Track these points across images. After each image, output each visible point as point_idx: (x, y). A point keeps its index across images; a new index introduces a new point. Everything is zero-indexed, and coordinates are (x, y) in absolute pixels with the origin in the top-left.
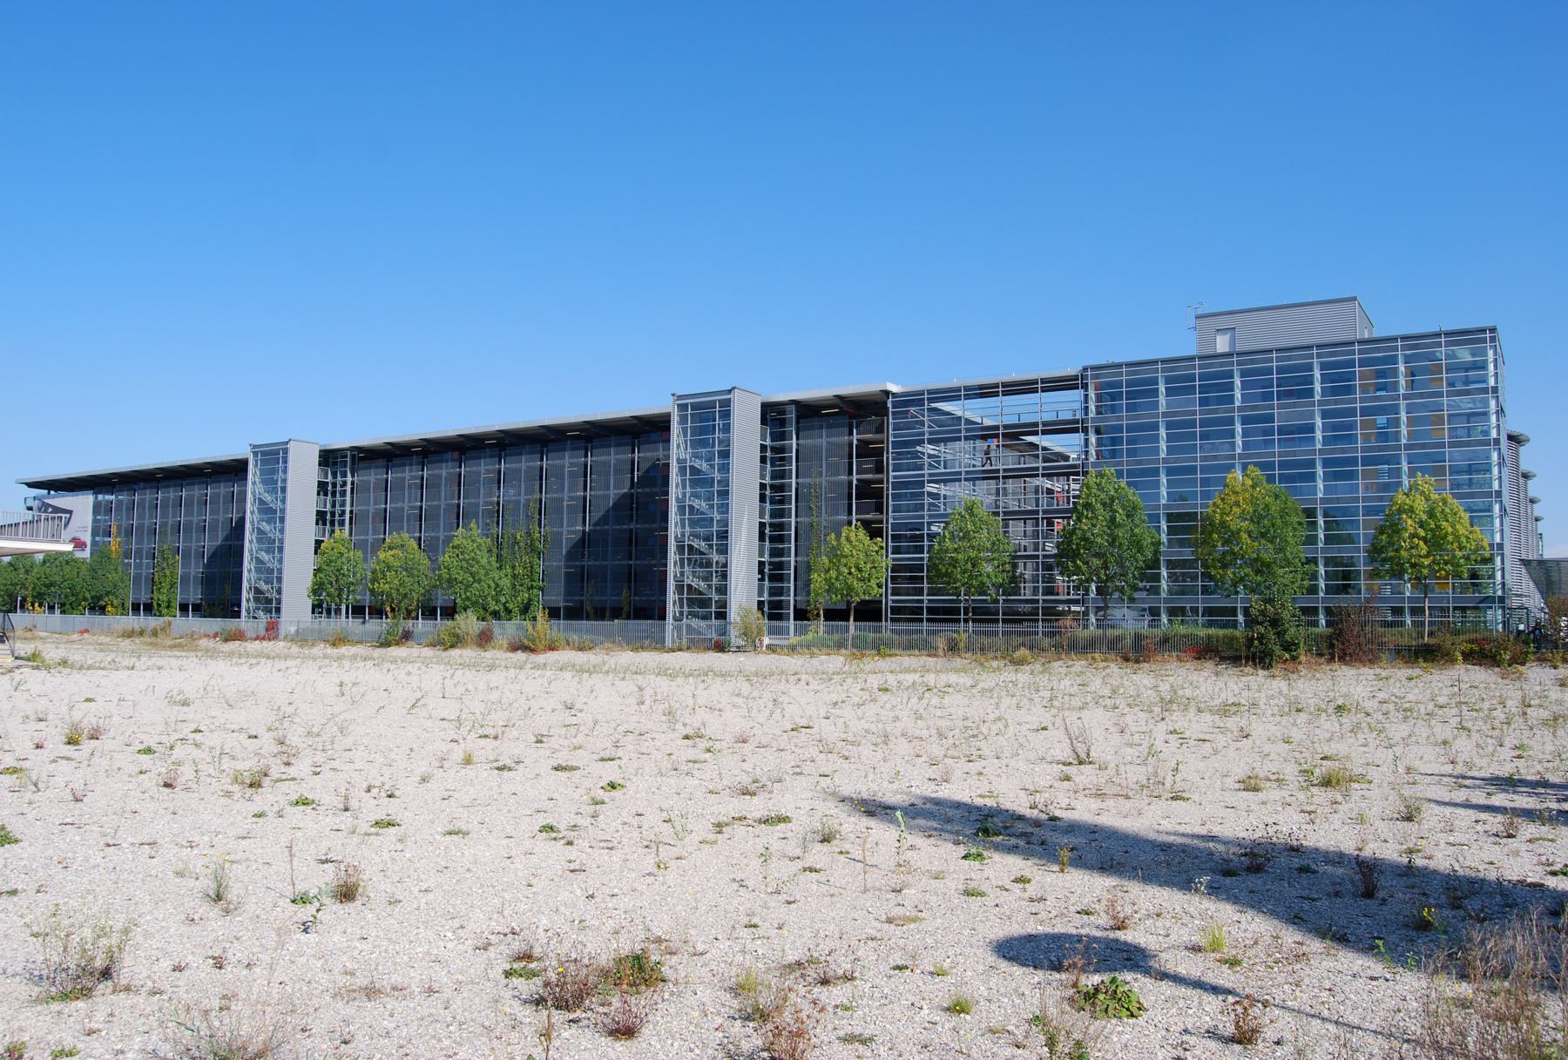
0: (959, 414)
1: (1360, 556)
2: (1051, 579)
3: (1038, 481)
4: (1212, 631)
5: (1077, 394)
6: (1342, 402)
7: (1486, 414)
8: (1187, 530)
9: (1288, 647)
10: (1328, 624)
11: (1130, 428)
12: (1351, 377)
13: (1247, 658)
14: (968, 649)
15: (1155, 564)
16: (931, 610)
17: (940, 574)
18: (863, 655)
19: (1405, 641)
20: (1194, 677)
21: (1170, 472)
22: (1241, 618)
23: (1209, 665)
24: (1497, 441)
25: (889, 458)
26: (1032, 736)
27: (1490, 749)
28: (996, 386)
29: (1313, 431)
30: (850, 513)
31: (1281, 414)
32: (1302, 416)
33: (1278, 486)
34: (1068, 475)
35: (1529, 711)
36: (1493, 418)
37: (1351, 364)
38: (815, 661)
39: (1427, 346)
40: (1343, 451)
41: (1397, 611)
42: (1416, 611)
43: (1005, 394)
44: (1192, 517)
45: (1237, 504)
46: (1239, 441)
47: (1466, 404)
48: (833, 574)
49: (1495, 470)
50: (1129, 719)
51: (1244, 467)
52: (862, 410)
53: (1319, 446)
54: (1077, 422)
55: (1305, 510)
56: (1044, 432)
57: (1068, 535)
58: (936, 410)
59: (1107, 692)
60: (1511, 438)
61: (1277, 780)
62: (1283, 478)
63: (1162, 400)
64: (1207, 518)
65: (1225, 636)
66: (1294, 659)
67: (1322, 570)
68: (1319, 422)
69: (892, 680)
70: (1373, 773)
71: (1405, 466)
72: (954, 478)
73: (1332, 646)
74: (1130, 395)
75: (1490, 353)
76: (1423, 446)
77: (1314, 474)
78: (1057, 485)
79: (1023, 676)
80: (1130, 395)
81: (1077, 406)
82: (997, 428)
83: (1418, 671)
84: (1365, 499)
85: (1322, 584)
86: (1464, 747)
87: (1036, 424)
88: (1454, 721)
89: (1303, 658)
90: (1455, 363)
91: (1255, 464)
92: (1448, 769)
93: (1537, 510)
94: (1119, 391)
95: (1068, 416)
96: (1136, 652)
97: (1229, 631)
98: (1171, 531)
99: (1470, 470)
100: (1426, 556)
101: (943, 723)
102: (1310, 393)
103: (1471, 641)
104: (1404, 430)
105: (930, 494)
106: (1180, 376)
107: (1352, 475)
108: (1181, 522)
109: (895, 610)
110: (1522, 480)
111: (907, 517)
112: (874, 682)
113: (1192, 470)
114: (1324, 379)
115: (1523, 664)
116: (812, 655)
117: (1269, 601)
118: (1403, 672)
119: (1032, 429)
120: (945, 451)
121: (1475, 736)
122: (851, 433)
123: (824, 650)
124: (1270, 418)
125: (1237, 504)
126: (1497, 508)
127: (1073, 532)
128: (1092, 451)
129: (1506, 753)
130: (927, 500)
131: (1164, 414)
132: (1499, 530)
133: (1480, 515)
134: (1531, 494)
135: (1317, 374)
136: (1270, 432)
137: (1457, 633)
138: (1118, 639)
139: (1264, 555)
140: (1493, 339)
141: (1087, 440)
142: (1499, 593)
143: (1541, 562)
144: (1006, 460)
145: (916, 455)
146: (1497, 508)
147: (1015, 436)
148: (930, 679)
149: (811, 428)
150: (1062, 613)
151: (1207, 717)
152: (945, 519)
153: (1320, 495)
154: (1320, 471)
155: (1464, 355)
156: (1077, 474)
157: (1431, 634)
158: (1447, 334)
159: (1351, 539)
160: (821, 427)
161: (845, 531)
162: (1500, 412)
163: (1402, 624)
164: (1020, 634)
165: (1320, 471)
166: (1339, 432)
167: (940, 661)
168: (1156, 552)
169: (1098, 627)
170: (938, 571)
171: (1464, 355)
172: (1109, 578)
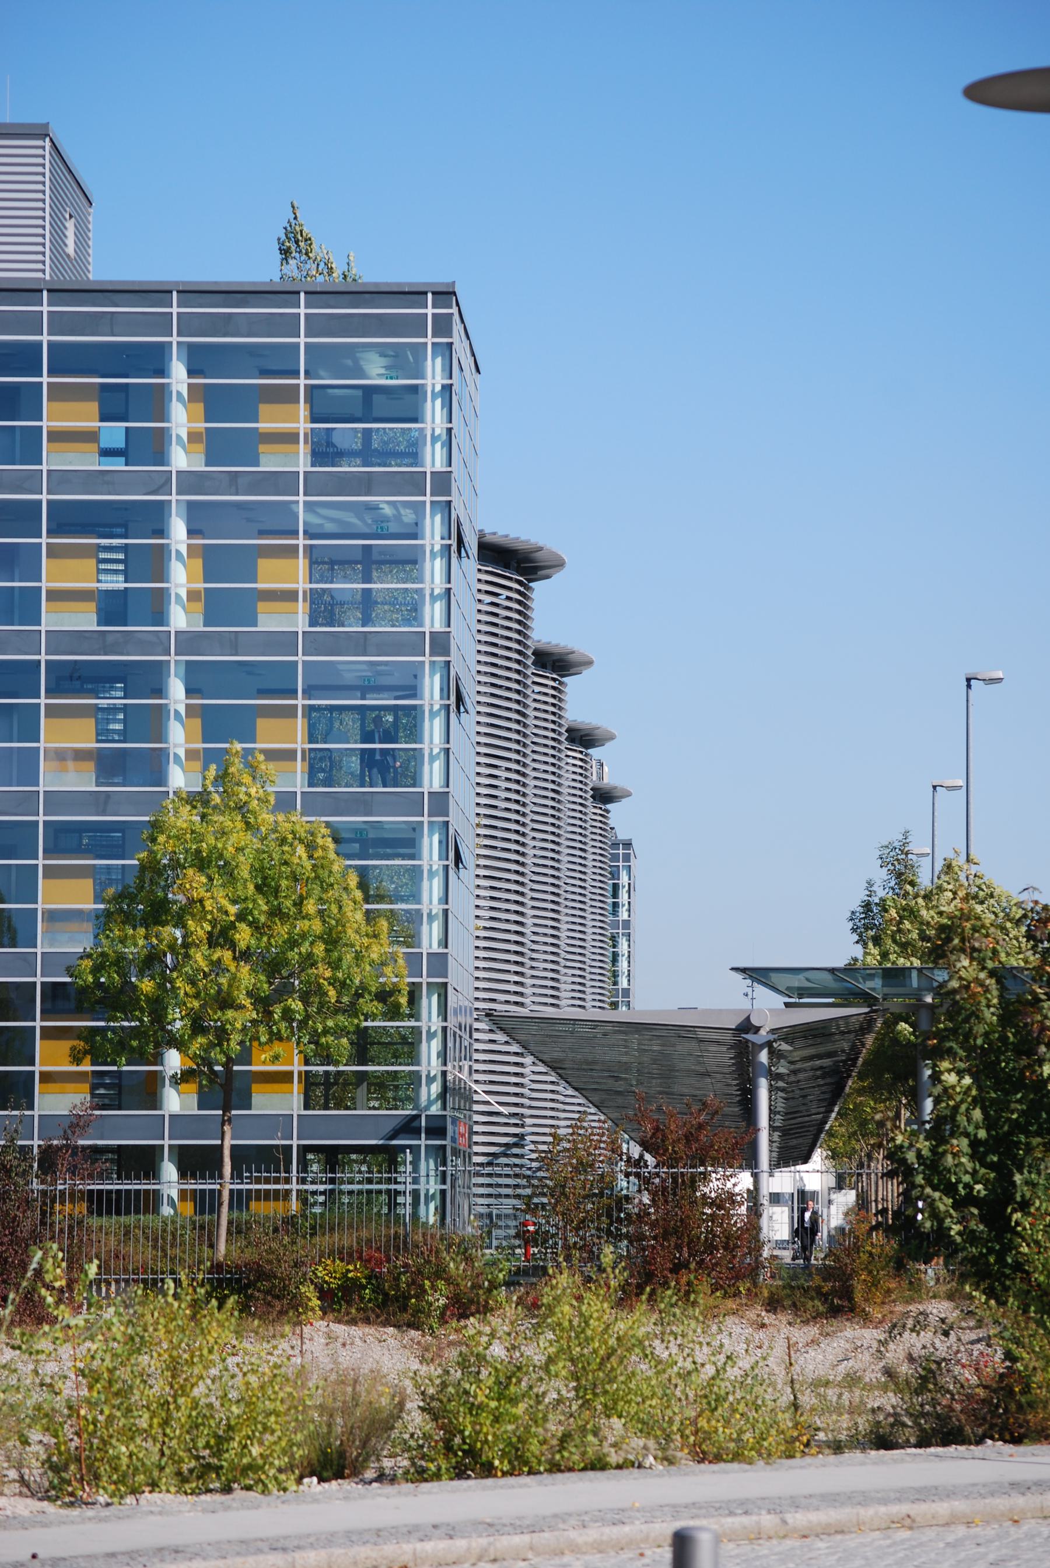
49: (433, 731)
163: (151, 1202)
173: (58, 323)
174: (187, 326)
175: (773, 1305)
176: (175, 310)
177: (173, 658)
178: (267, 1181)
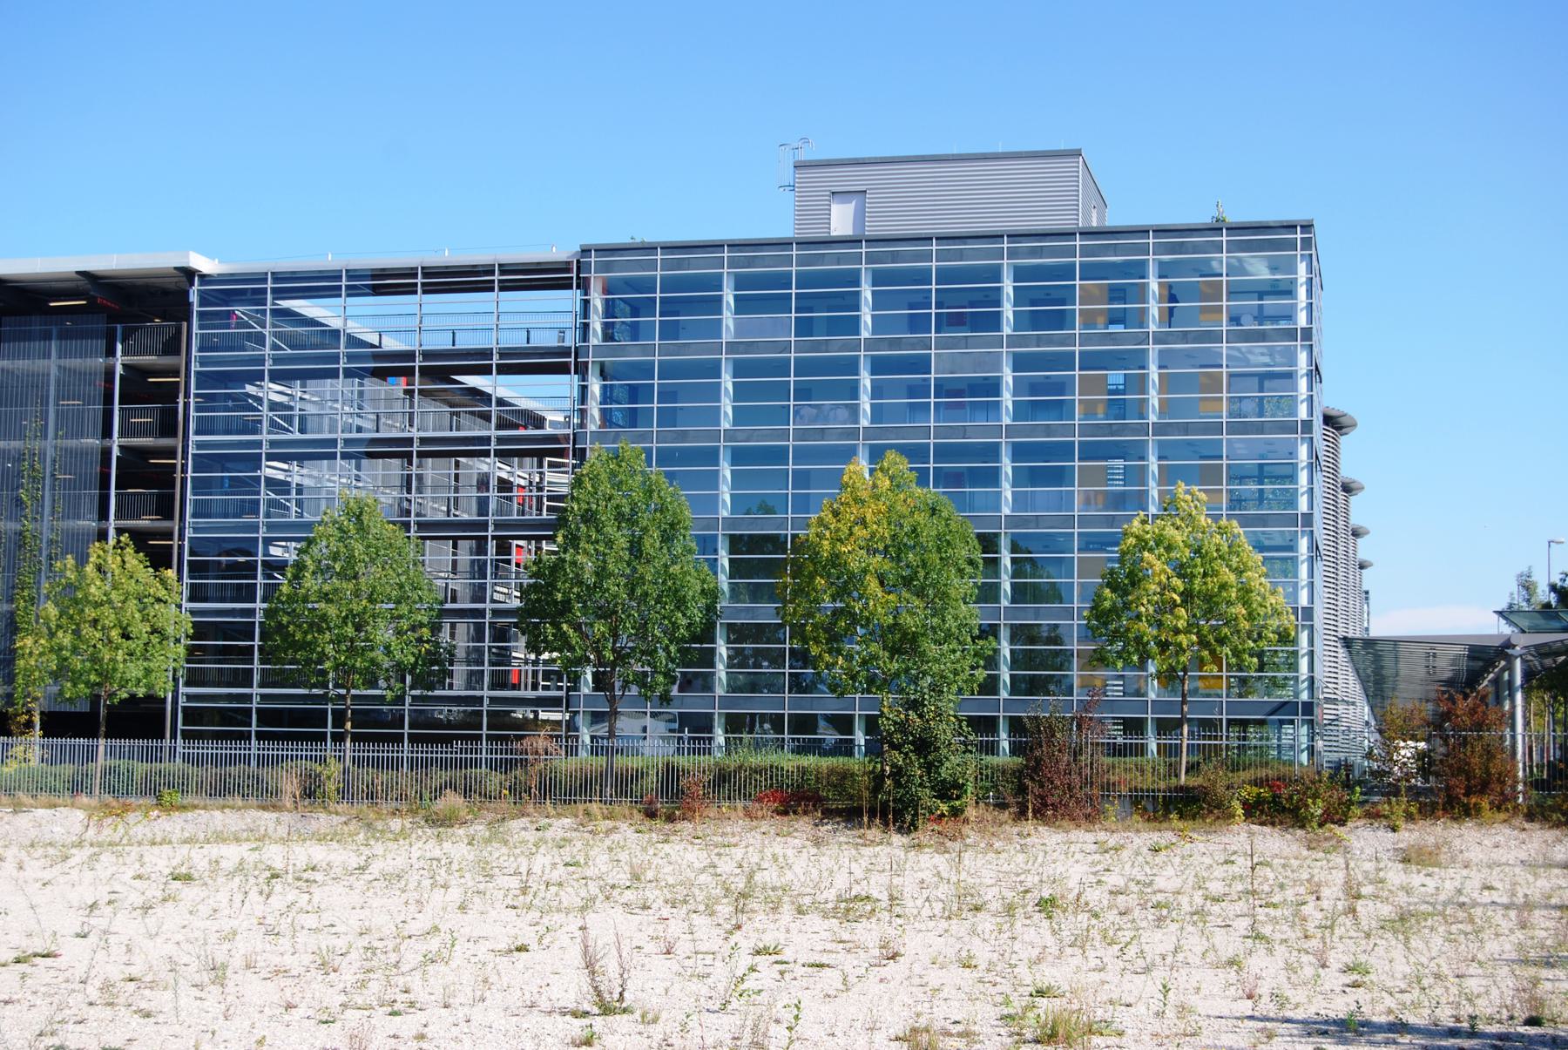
0: (335, 324)
1: (1072, 618)
2: (503, 657)
3: (483, 466)
4: (810, 761)
5: (567, 300)
6: (1050, 341)
7: (1290, 376)
8: (772, 568)
9: (948, 790)
10: (1016, 750)
11: (668, 370)
12: (1066, 296)
13: (872, 815)
14: (345, 793)
15: (707, 634)
16: (265, 717)
17: (286, 643)
18: (126, 808)
19: (1147, 782)
20: (777, 846)
21: (738, 456)
22: (860, 738)
23: (803, 825)
24: (1307, 426)
25: (189, 405)
26: (504, 961)
27: (1308, 972)
28: (411, 273)
29: (997, 393)
30: (103, 515)
31: (944, 356)
32: (979, 363)
33: (932, 492)
34: (540, 455)
35: (1359, 905)
36: (1303, 384)
37: (1067, 272)
38: (23, 820)
39: (1196, 248)
40: (1048, 431)
41: (1134, 726)
42: (1164, 727)
43: (429, 289)
44: (776, 543)
45: (863, 522)
46: (865, 403)
47: (1259, 356)
48: (66, 639)
49: (1303, 477)
50: (676, 928)
51: (876, 454)
52: (135, 306)
53: (1006, 420)
54: (565, 352)
55: (981, 538)
56: (504, 370)
57: (547, 577)
58: (287, 313)
59: (623, 878)
60: (1329, 420)
61: (965, 1034)
62: (944, 478)
63: (728, 318)
64: (799, 545)
65: (832, 771)
66: (956, 813)
67: (1006, 649)
68: (1008, 376)
69: (199, 859)
70: (1124, 1018)
71: (1153, 464)
72: (320, 452)
73: (1022, 790)
74: (669, 307)
75: (1302, 268)
76: (1186, 429)
77: (997, 471)
78: (520, 474)
79: (456, 847)
80: (669, 307)
81: (568, 321)
82: (410, 356)
83: (1169, 836)
84: (1083, 521)
85: (1005, 675)
86: (1266, 968)
87: (487, 353)
88: (1243, 924)
89: (971, 812)
90: (1245, 275)
91: (903, 450)
92: (1246, 1007)
93: (1364, 549)
94: (648, 294)
95: (548, 340)
96: (668, 800)
97: (838, 762)
98: (737, 569)
99: (1261, 474)
100: (1187, 631)
101: (325, 940)
102: (994, 321)
103: (1257, 783)
104: (1154, 398)
105: (271, 482)
106: (764, 276)
107: (1059, 477)
108: (757, 554)
109: (191, 716)
110: (1341, 495)
111: (222, 528)
112: (161, 861)
113: (779, 455)
114: (1020, 296)
115: (1342, 823)
116: (18, 808)
117: (915, 705)
118: (1142, 838)
119: (478, 361)
120: (308, 398)
121: (1280, 950)
122: (111, 352)
123: (43, 797)
124: (922, 365)
125: (863, 522)
126: (1303, 544)
127: (557, 567)
128: (594, 409)
129: (1334, 979)
130: (265, 495)
131: (732, 347)
132: (1307, 585)
133: (1280, 558)
134: (1356, 520)
135: (1008, 286)
136: (920, 390)
137: (1235, 767)
138: (639, 775)
139: (908, 621)
140: (1307, 244)
141: (584, 390)
142: (1305, 696)
143: (1370, 643)
144: (431, 421)
145: (244, 402)
146: (1303, 544)
147: (443, 374)
148: (274, 855)
149: (28, 337)
150: (524, 724)
151: (814, 921)
152: (305, 535)
153: (1006, 511)
154: (1007, 466)
155: (1259, 269)
156: (561, 453)
157: (1192, 768)
158: (1233, 229)
159: (1056, 594)
160: (47, 337)
161: (95, 549)
162: (1315, 373)
163: (1141, 750)
164: (444, 764)
165: (1007, 466)
166: (1043, 397)
167: (286, 817)
168: (710, 609)
169: (594, 751)
170: (287, 636)
171: (1259, 269)
172: (621, 657)
173: (1086, 251)
174: (871, 258)
175: (1530, 817)
176: (1078, 243)
177: (1151, 438)
178: (1210, 738)
